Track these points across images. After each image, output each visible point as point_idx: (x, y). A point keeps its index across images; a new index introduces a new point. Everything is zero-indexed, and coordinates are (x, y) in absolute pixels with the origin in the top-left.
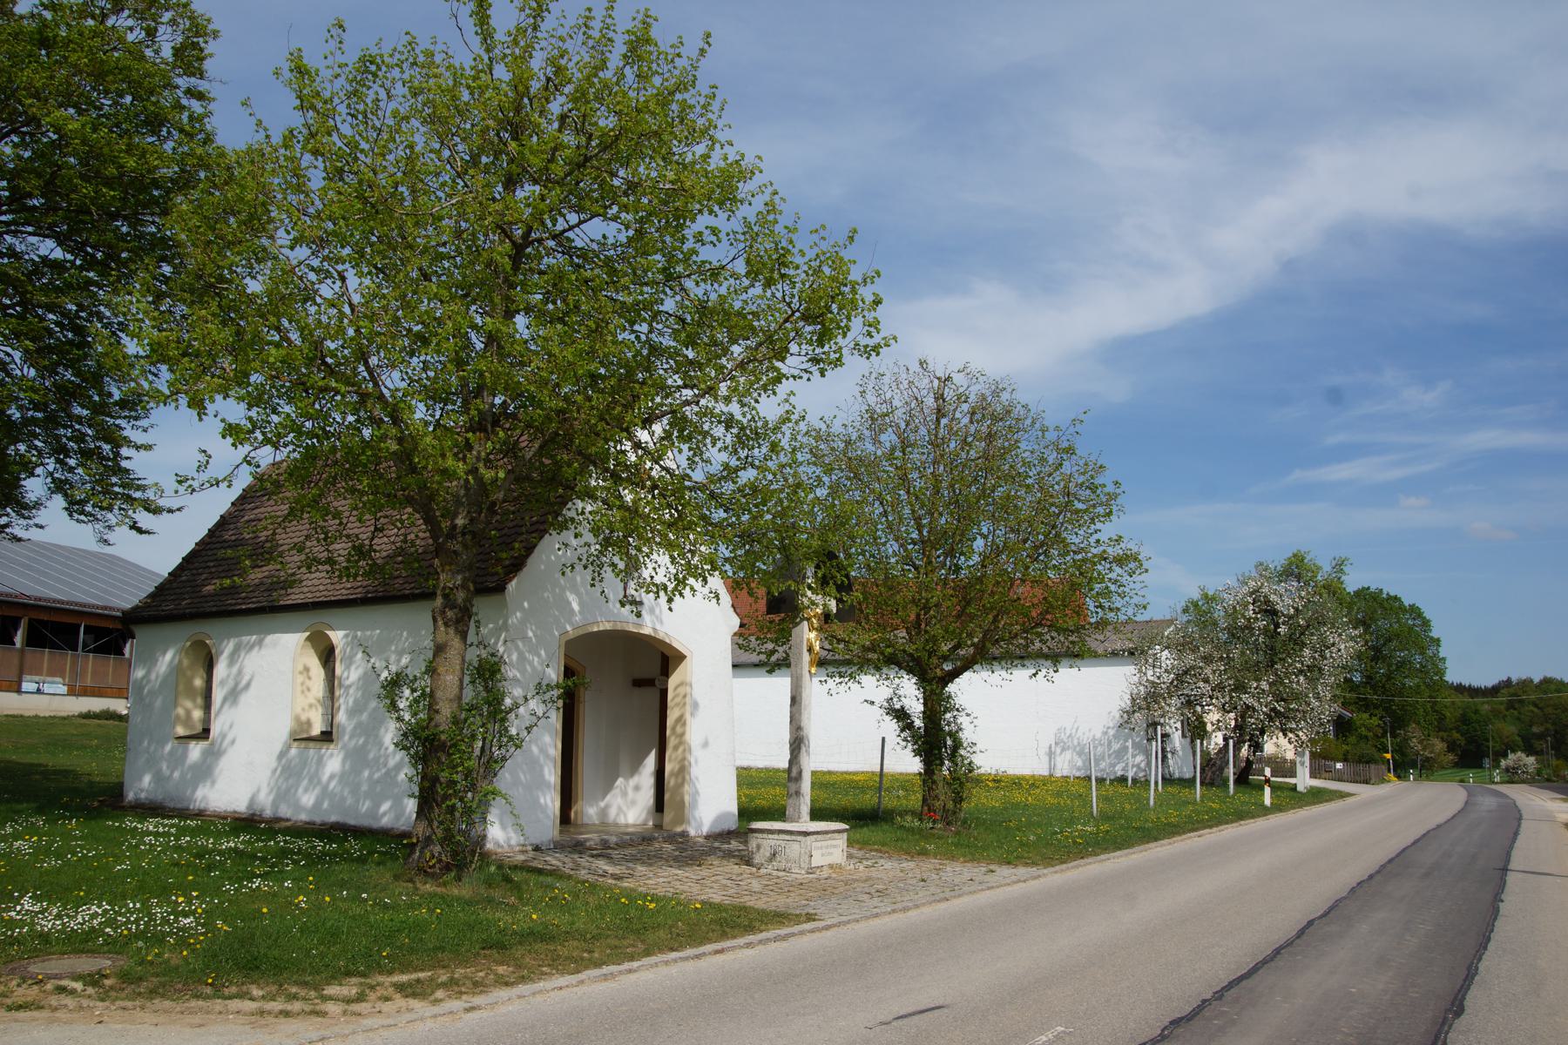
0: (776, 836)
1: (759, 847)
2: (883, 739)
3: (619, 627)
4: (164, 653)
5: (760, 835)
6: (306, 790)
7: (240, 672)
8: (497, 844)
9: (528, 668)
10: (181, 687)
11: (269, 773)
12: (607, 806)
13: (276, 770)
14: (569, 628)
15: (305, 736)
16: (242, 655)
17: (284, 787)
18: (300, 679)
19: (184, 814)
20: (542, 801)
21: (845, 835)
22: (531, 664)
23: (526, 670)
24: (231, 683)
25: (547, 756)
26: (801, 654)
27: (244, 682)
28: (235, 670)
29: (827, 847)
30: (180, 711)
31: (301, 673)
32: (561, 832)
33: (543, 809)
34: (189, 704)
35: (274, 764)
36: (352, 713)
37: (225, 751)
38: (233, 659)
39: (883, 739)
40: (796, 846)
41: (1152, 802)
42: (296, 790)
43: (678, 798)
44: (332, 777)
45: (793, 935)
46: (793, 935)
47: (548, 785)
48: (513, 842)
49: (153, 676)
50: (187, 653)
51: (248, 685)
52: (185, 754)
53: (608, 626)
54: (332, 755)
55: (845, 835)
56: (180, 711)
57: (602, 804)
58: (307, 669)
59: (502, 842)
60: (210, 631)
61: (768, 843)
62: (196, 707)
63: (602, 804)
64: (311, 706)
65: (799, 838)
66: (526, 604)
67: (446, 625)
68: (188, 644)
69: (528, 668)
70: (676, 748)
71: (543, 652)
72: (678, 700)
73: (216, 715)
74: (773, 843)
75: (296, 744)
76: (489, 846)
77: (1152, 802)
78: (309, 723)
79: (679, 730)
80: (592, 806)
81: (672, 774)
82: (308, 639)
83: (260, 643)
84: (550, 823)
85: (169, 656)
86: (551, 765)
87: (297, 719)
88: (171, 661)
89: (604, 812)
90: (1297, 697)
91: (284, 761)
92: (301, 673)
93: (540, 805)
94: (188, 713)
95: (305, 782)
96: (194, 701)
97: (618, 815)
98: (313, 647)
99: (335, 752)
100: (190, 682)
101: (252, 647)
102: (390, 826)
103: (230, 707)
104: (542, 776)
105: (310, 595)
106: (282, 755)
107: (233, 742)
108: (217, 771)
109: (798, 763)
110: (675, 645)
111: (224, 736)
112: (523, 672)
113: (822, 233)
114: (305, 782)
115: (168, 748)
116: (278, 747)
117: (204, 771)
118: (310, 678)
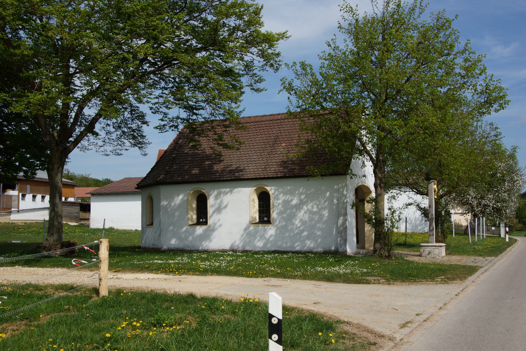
0: (430, 247)
1: (424, 251)
4: (178, 196)
5: (424, 247)
6: (259, 241)
7: (221, 202)
10: (189, 207)
11: (240, 236)
13: (243, 234)
15: (254, 222)
16: (222, 196)
17: (248, 240)
18: (252, 203)
19: (198, 251)
24: (217, 206)
26: (432, 192)
27: (224, 205)
28: (218, 201)
30: (189, 216)
34: (191, 213)
35: (242, 232)
36: (279, 214)
37: (217, 229)
38: (216, 197)
40: (437, 250)
41: (476, 240)
42: (254, 241)
44: (271, 236)
49: (173, 204)
50: (191, 195)
51: (226, 207)
52: (194, 231)
54: (270, 229)
55: (445, 247)
56: (189, 216)
58: (254, 200)
60: (205, 188)
61: (428, 250)
62: (194, 214)
64: (255, 212)
65: (438, 248)
67: (381, 188)
68: (192, 192)
73: (210, 217)
74: (429, 250)
75: (253, 225)
77: (476, 240)
78: (255, 218)
81: (367, 230)
82: (255, 190)
83: (231, 192)
85: (181, 197)
87: (252, 217)
88: (182, 199)
90: (504, 201)
91: (247, 232)
94: (192, 217)
95: (258, 238)
96: (193, 212)
98: (256, 192)
99: (272, 227)
100: (191, 206)
101: (227, 193)
102: (300, 250)
103: (217, 214)
105: (250, 175)
106: (246, 229)
107: (220, 226)
108: (212, 237)
111: (215, 224)
113: (499, 81)
114: (258, 238)
115: (184, 229)
116: (244, 226)
117: (206, 236)
118: (254, 203)
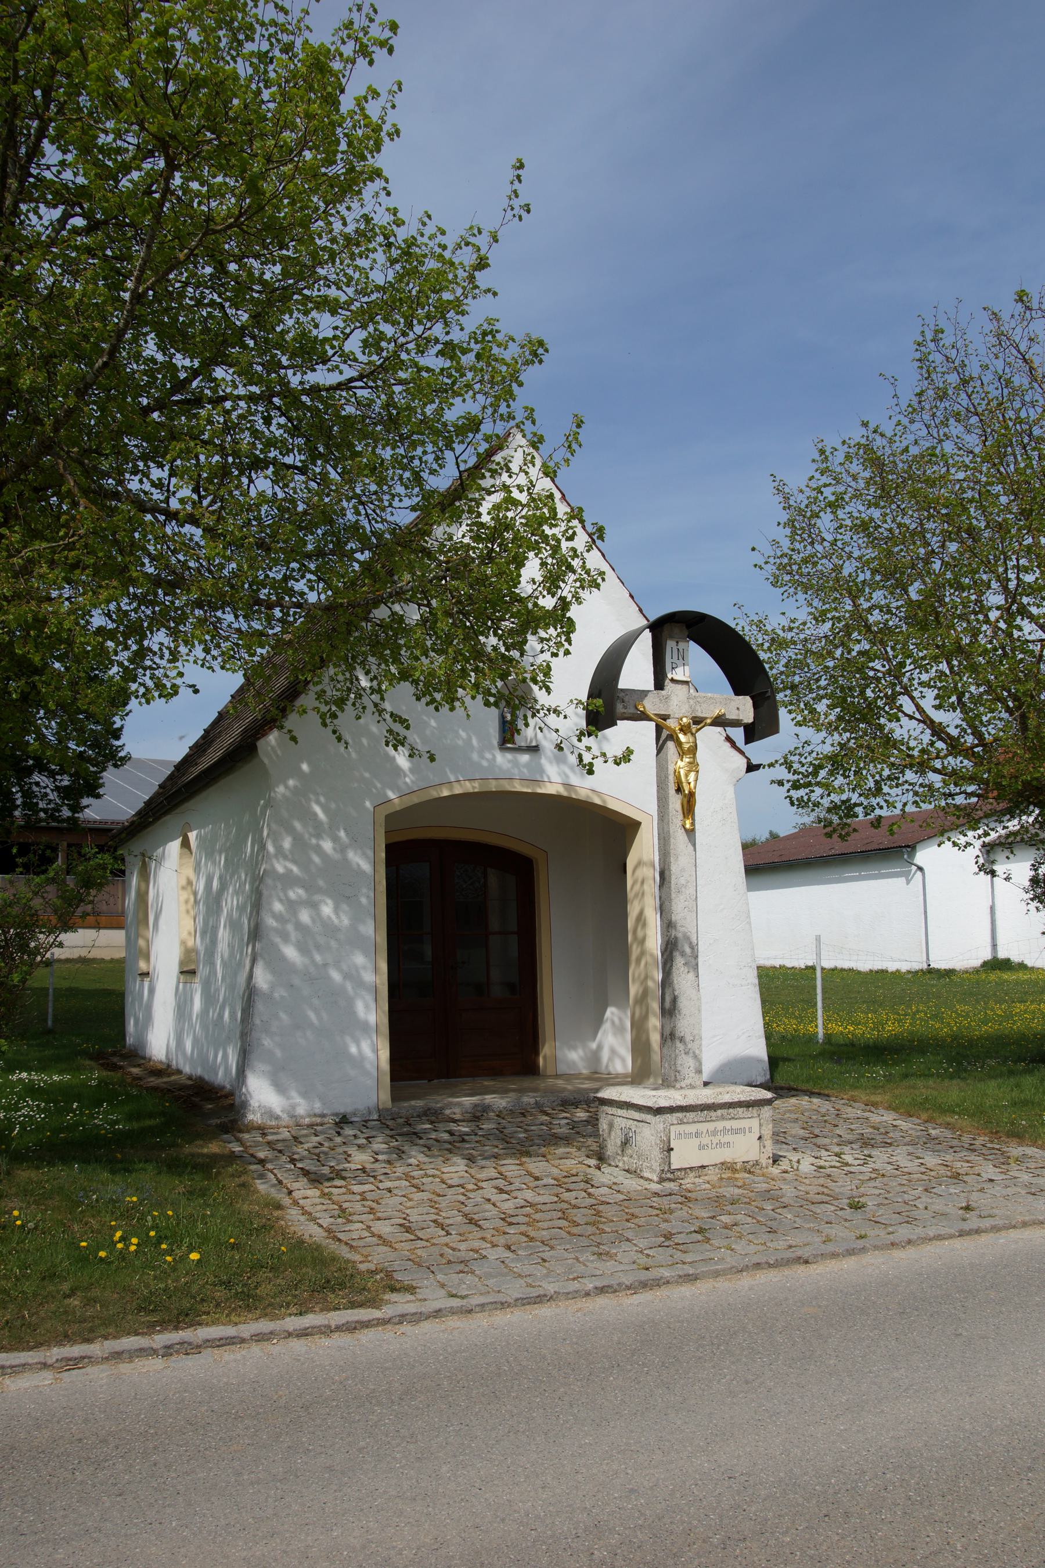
2: (818, 939)
3: (493, 786)
8: (270, 1113)
9: (316, 859)
12: (600, 1047)
14: (391, 795)
20: (353, 1049)
21: (766, 1112)
22: (319, 850)
23: (310, 861)
25: (360, 983)
29: (715, 1133)
31: (183, 888)
32: (395, 1097)
33: (358, 1062)
39: (818, 939)
43: (644, 1038)
45: (366, 1325)
46: (366, 1325)
47: (365, 1027)
48: (301, 1110)
53: (469, 787)
57: (594, 1046)
59: (278, 1111)
63: (594, 1046)
65: (648, 1117)
66: (305, 767)
69: (316, 859)
70: (638, 961)
71: (342, 834)
72: (637, 887)
76: (253, 1117)
79: (640, 934)
80: (574, 1048)
84: (371, 1083)
86: (370, 998)
89: (595, 1057)
92: (183, 888)
93: (350, 1057)
97: (610, 1059)
104: (353, 1013)
109: (671, 984)
110: (613, 805)
112: (305, 864)
